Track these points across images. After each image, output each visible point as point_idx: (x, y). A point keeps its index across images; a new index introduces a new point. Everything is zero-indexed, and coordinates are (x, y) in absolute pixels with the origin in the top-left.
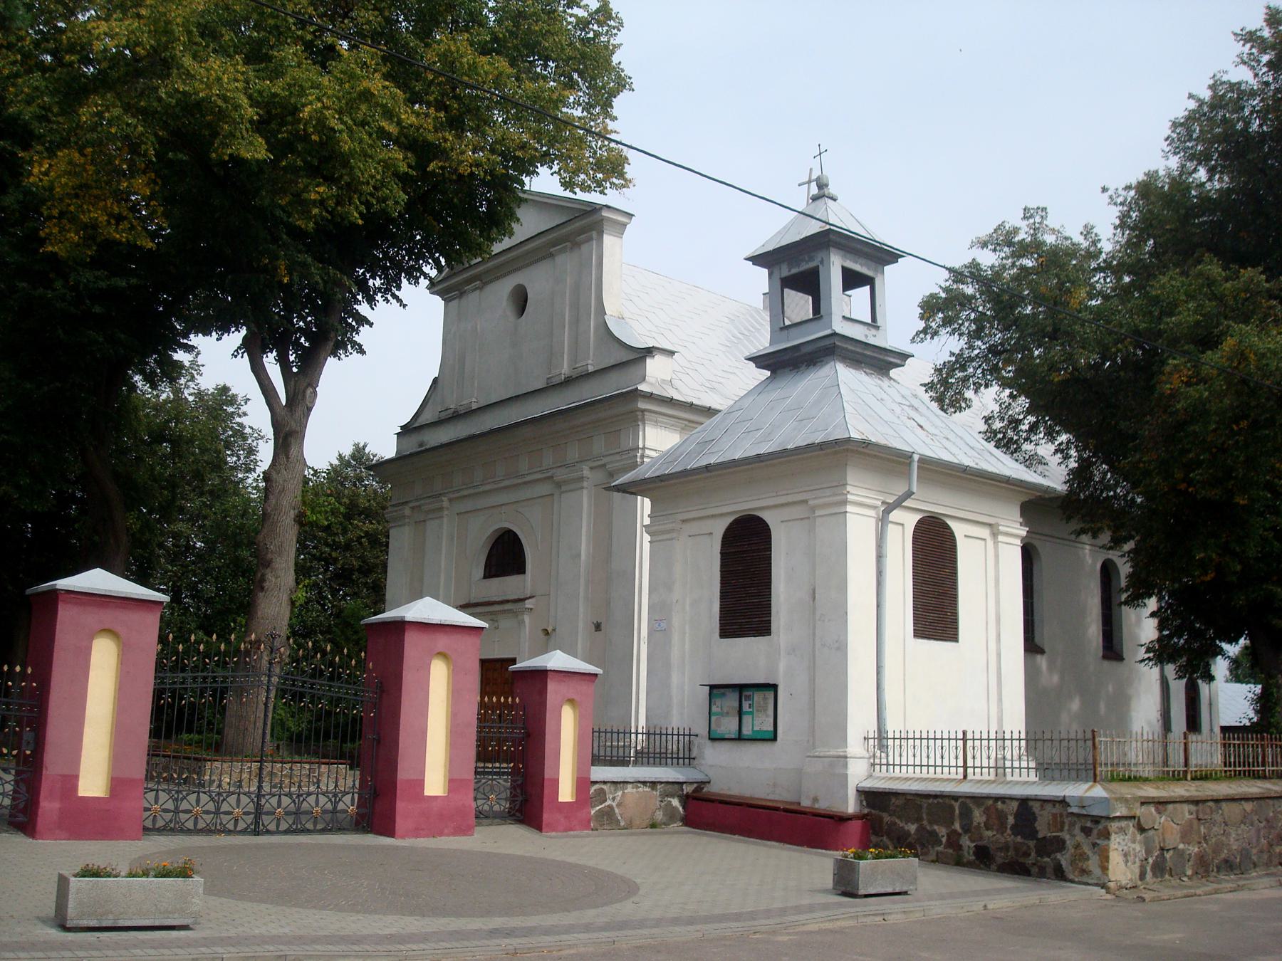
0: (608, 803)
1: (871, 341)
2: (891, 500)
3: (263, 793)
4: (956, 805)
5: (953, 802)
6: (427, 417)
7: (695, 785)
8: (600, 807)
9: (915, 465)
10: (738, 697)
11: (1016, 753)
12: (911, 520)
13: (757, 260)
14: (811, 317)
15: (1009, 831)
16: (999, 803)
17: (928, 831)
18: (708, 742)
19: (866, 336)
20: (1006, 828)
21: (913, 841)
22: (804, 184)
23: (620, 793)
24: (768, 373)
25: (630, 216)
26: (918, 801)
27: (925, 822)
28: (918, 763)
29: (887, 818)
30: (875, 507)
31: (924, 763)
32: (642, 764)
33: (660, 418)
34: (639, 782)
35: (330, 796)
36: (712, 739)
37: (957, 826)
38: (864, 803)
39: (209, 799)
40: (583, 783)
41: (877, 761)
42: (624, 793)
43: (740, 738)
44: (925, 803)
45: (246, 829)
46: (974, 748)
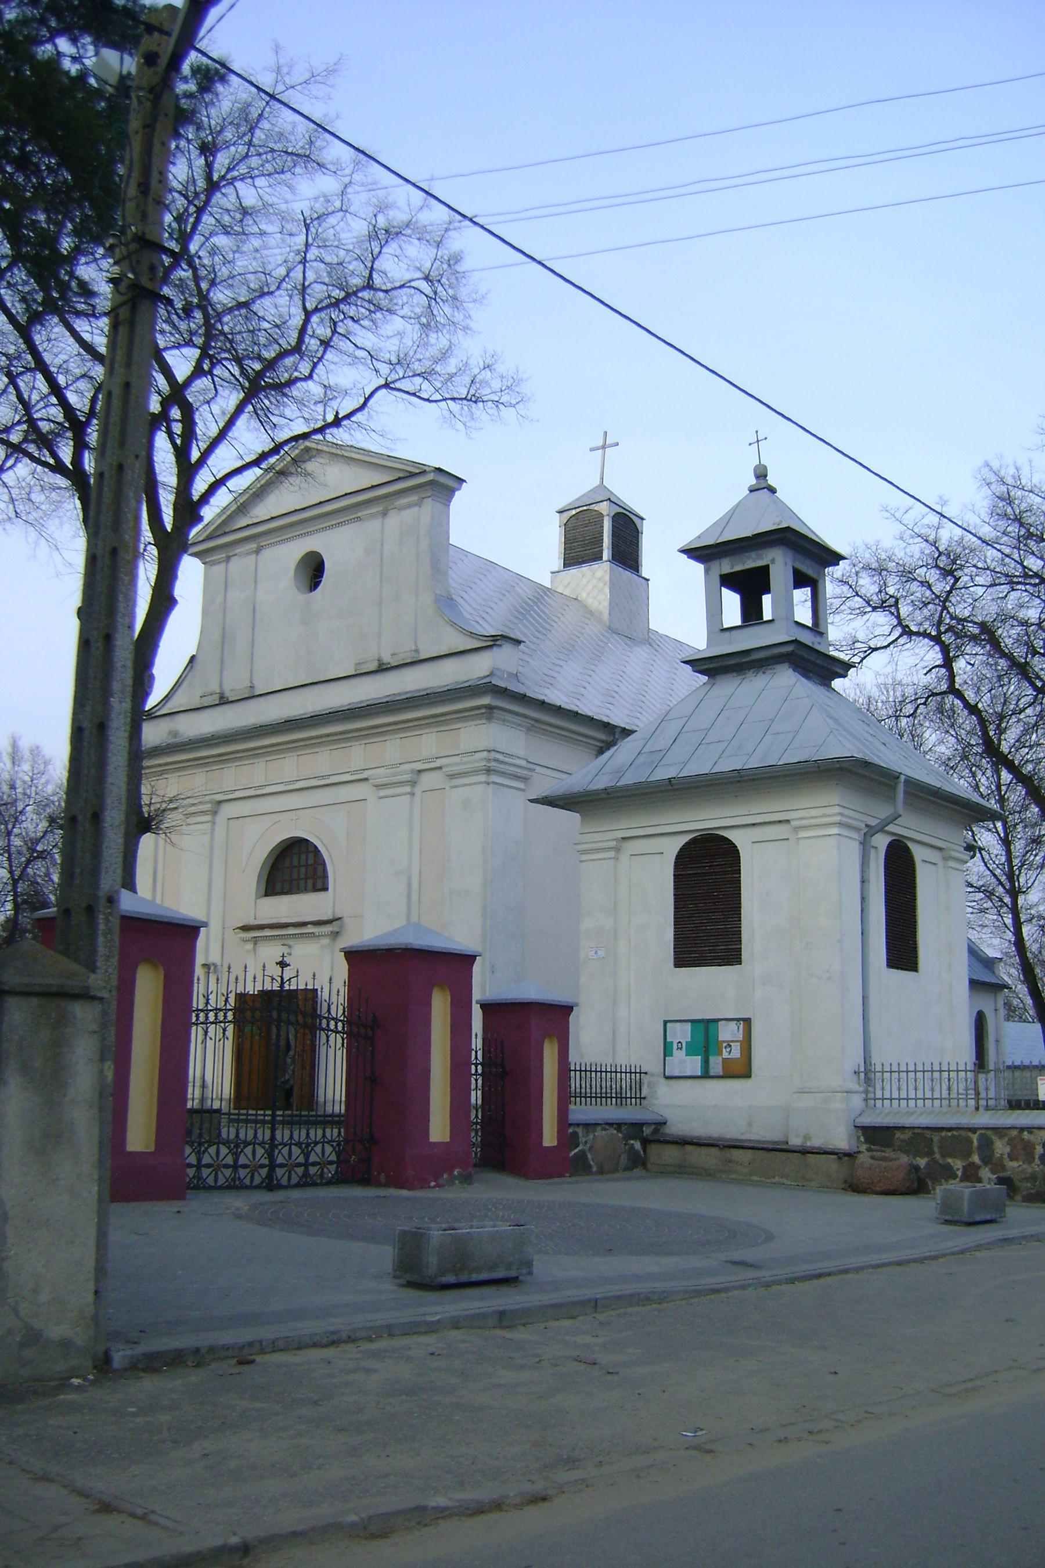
3: (276, 1142)
4: (975, 1138)
5: (970, 1134)
7: (653, 1127)
8: (576, 1151)
9: (901, 788)
11: (962, 1086)
12: (887, 839)
13: (695, 553)
14: (739, 623)
15: (1037, 1161)
16: (1026, 1133)
17: (940, 1165)
18: (662, 1080)
19: (813, 643)
20: (1034, 1159)
21: (923, 1176)
22: (597, 449)
25: (461, 481)
27: (937, 1156)
28: (887, 1095)
30: (858, 830)
31: (912, 1095)
33: (509, 717)
34: (607, 1124)
37: (976, 1159)
38: (862, 1139)
41: (871, 1095)
42: (595, 1137)
46: (916, 1081)
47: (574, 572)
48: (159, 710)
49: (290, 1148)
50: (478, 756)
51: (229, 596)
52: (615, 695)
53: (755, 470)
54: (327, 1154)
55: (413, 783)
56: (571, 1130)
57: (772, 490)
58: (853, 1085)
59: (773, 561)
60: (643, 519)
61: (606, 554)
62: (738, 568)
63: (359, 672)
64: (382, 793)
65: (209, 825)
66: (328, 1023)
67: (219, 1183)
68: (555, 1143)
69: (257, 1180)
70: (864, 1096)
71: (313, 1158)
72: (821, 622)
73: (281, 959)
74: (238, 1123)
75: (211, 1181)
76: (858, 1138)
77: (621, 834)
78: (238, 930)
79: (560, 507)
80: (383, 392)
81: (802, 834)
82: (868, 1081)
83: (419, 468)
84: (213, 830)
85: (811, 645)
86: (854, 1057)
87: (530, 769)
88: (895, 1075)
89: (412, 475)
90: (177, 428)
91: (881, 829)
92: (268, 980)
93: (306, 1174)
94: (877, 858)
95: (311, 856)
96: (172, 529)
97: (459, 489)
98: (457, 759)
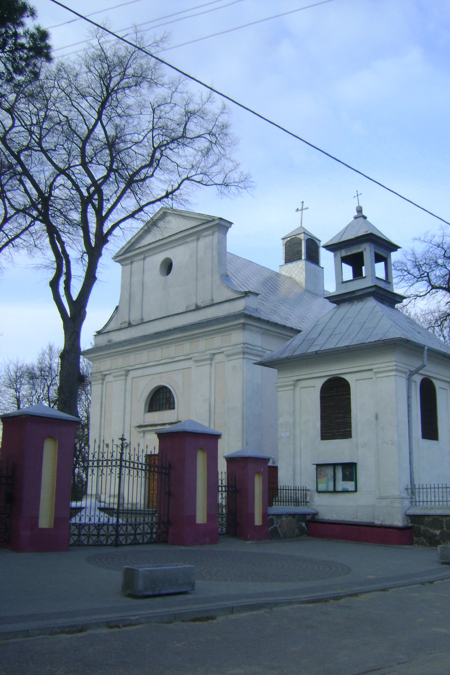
0: (275, 525)
1: (388, 289)
2: (413, 369)
6: (112, 326)
7: (311, 516)
8: (272, 528)
9: (425, 352)
10: (333, 470)
18: (316, 494)
19: (385, 287)
23: (280, 520)
24: (336, 305)
25: (231, 223)
26: (440, 519)
27: (445, 529)
28: (421, 500)
29: (422, 528)
30: (406, 373)
31: (433, 499)
32: (299, 505)
33: (253, 328)
35: (150, 525)
36: (319, 492)
38: (409, 521)
39: (132, 528)
40: (265, 515)
42: (282, 520)
43: (335, 491)
44: (444, 520)
45: (112, 543)
47: (290, 265)
48: (103, 330)
49: (144, 525)
50: (239, 346)
51: (133, 279)
52: (305, 318)
53: (357, 209)
54: (145, 529)
55: (211, 359)
56: (270, 517)
57: (365, 218)
58: (405, 495)
59: (365, 249)
60: (320, 241)
61: (303, 257)
62: (349, 253)
63: (187, 310)
64: (198, 364)
65: (124, 381)
66: (138, 466)
67: (90, 543)
68: (260, 524)
69: (110, 542)
70: (410, 500)
71: (139, 531)
72: (389, 278)
73: (121, 437)
74: (123, 514)
75: (86, 542)
76: (408, 521)
77: (296, 378)
78: (136, 428)
79: (282, 237)
80: (186, 182)
81: (379, 375)
82: (413, 493)
83: (212, 218)
84: (126, 383)
85: (384, 288)
86: (406, 481)
87: (264, 352)
88: (425, 490)
89: (209, 222)
90: (96, 203)
91: (416, 372)
92: (115, 447)
93: (135, 539)
94: (416, 386)
95: (168, 394)
96: (94, 246)
97: (230, 227)
98: (230, 348)
